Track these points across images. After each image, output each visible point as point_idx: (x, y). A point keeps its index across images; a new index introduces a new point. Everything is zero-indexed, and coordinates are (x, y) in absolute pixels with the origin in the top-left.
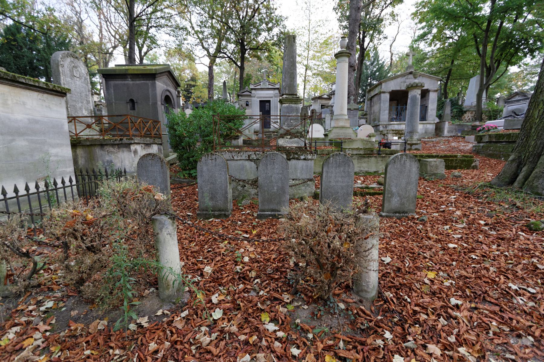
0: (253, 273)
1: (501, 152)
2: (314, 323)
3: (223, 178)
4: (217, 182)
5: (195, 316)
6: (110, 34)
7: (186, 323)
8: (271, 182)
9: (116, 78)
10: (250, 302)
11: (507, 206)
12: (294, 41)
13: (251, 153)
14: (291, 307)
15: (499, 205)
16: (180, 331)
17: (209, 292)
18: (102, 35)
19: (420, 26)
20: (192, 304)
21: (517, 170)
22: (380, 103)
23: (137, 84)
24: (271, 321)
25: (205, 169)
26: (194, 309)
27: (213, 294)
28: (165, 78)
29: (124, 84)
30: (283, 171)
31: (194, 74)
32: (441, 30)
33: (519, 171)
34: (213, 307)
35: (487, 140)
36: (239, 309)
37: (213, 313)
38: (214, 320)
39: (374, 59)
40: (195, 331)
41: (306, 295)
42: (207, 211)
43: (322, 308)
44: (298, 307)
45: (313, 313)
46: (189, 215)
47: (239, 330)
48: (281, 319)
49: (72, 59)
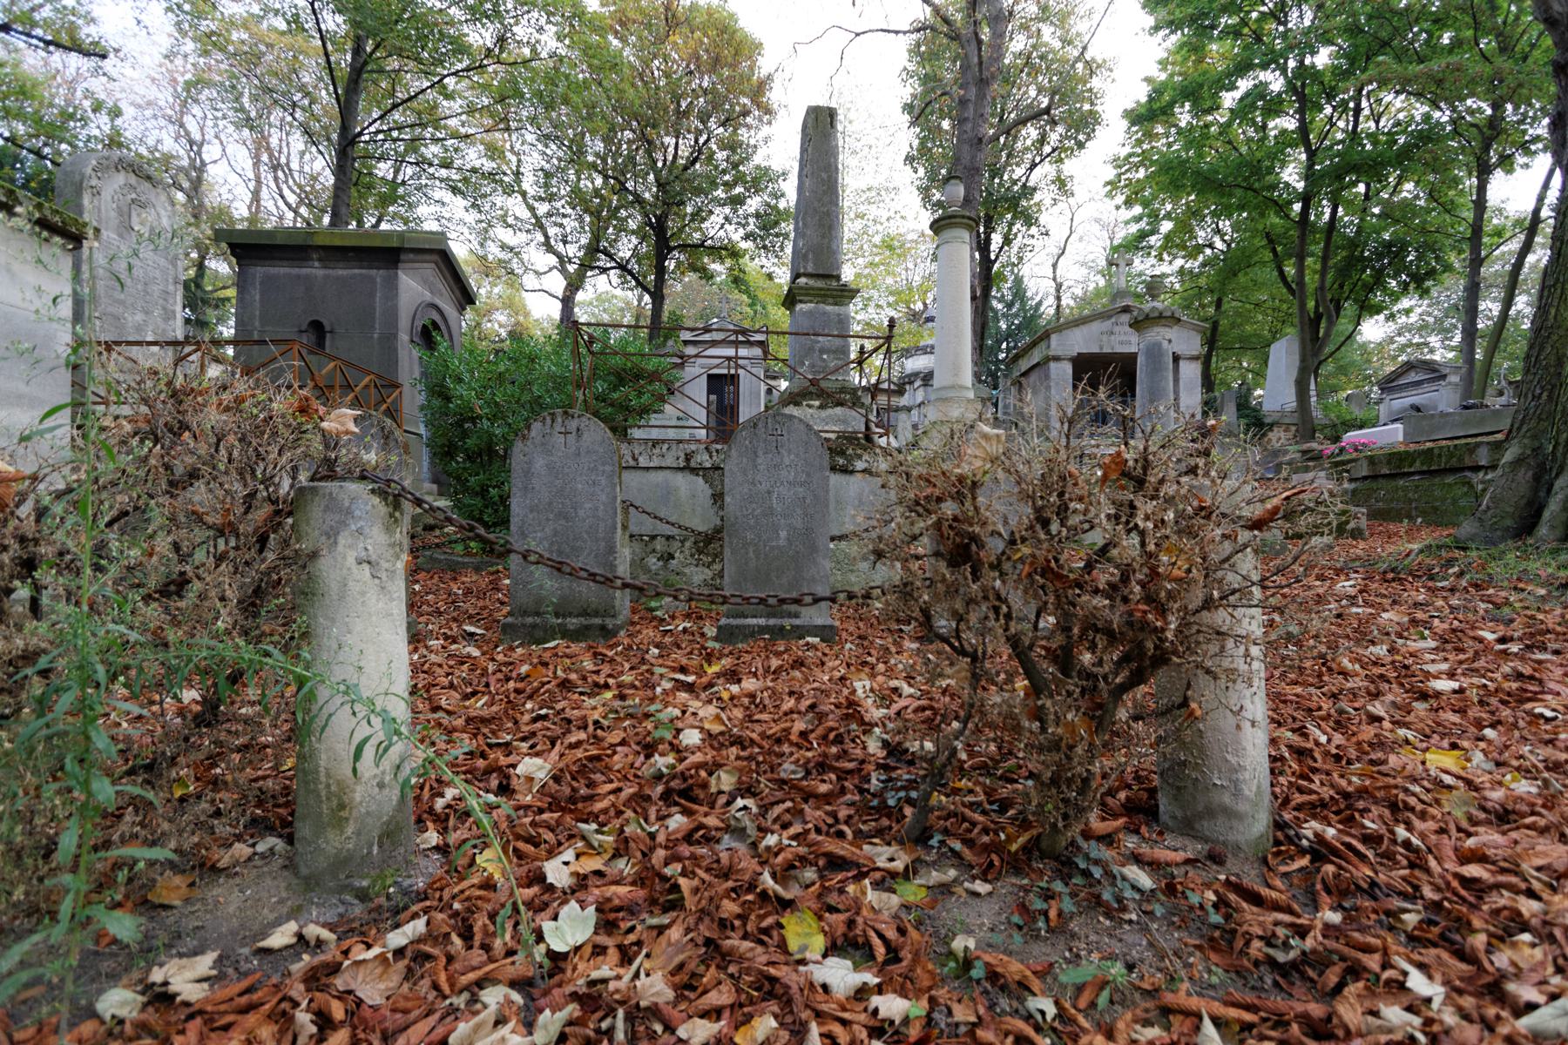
0: (724, 776)
1: (1410, 501)
2: (1042, 953)
3: (603, 497)
4: (581, 513)
5: (457, 941)
6: (281, 203)
7: (409, 974)
8: (770, 512)
9: (273, 258)
10: (725, 875)
11: (1543, 592)
12: (832, 125)
13: (693, 447)
14: (913, 892)
15: (1515, 588)
16: (367, 1013)
17: (527, 847)
18: (258, 206)
19: (1126, 214)
20: (446, 894)
21: (1536, 490)
22: (1048, 388)
23: (338, 278)
24: (832, 950)
25: (540, 463)
26: (456, 914)
27: (551, 854)
28: (429, 270)
29: (298, 277)
30: (808, 475)
31: (518, 323)
32: (1184, 227)
33: (1542, 494)
34: (547, 899)
35: (1364, 473)
36: (675, 905)
37: (547, 926)
38: (552, 955)
39: (1015, 295)
40: (453, 1011)
41: (969, 843)
42: (538, 614)
43: (1058, 886)
44: (945, 889)
45: (1023, 908)
46: (472, 634)
47: (680, 998)
48: (881, 936)
49: (133, 179)
